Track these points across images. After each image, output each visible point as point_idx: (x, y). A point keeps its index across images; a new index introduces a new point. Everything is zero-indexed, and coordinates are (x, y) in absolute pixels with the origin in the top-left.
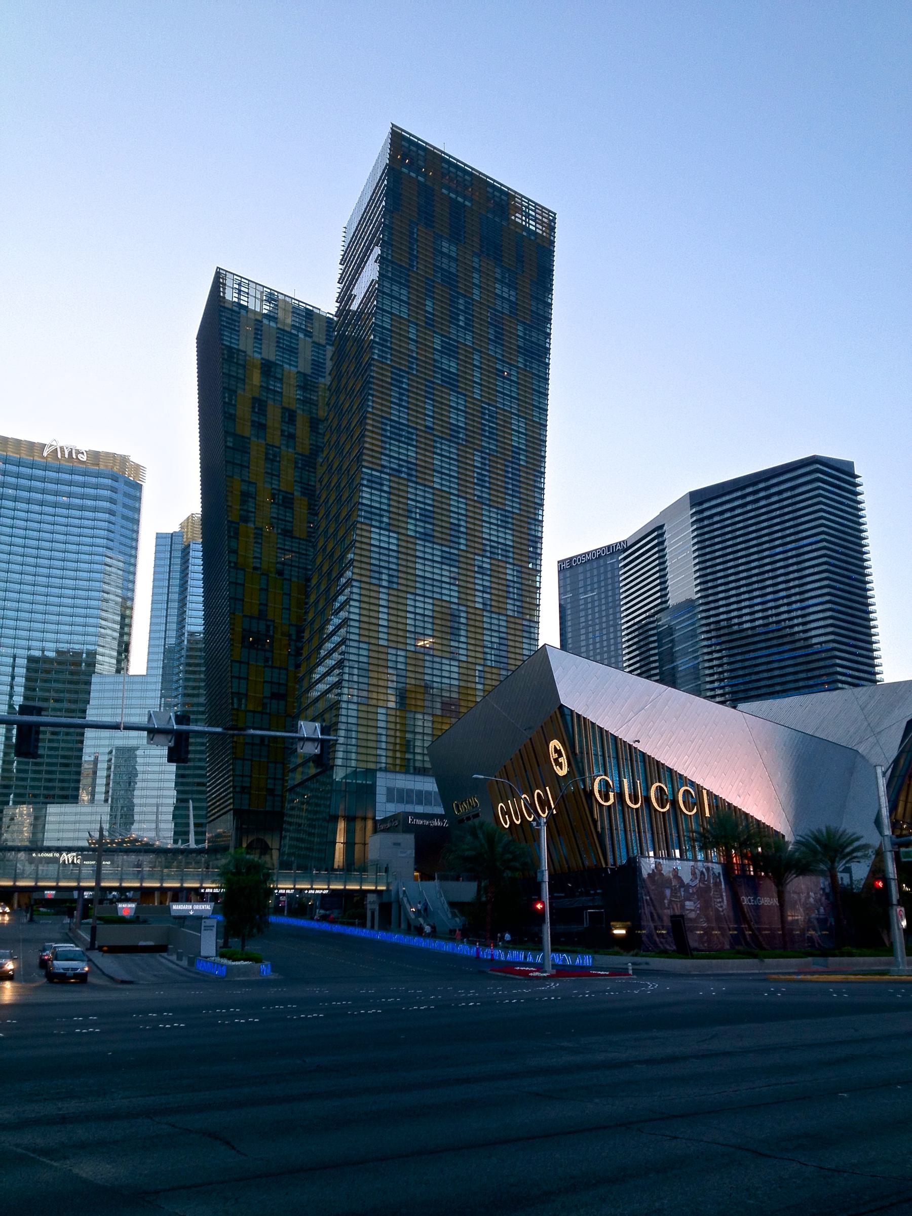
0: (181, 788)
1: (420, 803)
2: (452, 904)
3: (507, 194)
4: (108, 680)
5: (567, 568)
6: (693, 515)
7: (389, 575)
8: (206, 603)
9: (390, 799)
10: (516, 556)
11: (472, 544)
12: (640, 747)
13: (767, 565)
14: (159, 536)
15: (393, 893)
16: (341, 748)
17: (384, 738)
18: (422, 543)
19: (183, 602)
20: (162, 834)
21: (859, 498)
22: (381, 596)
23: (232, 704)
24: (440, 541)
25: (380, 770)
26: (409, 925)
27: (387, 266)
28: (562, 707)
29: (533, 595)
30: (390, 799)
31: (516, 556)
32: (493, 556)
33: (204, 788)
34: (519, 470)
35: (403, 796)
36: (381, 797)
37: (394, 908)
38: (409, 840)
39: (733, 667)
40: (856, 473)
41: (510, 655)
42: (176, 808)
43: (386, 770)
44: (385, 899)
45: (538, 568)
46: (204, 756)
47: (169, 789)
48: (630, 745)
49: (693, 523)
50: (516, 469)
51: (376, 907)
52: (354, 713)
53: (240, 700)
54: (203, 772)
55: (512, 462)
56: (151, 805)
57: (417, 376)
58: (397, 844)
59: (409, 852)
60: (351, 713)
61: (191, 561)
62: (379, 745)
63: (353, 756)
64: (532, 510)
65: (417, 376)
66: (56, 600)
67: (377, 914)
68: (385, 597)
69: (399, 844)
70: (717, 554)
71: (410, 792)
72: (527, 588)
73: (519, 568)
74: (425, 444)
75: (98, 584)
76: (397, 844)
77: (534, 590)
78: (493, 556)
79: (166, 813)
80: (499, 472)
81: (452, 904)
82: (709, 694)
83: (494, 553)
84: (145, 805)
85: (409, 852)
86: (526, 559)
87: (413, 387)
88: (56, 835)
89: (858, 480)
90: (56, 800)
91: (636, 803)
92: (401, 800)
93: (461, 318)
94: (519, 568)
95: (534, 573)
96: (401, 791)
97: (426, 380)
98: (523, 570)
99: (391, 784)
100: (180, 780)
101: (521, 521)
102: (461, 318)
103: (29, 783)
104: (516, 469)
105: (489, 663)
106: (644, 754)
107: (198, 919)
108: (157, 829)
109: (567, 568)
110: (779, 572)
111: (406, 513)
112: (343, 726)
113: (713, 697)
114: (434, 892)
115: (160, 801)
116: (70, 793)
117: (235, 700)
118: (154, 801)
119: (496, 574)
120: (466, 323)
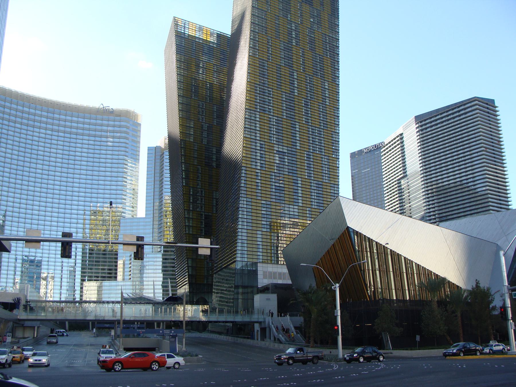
0: (165, 273)
1: (280, 279)
4: (128, 221)
5: (353, 155)
6: (417, 128)
7: (261, 144)
8: (172, 188)
9: (265, 277)
10: (326, 151)
11: (303, 146)
13: (458, 132)
14: (149, 149)
15: (267, 323)
16: (239, 252)
17: (261, 247)
18: (277, 146)
19: (161, 181)
20: (156, 295)
22: (258, 236)
23: (186, 231)
24: (286, 145)
25: (260, 262)
26: (275, 338)
27: (256, 35)
28: (348, 227)
29: (335, 162)
30: (265, 277)
31: (326, 151)
32: (314, 152)
33: (174, 273)
34: (326, 108)
35: (273, 275)
37: (267, 330)
38: (274, 297)
39: (441, 212)
40: (496, 105)
41: (324, 193)
42: (163, 282)
43: (262, 262)
44: (263, 326)
45: (338, 157)
46: (174, 257)
47: (159, 273)
48: (384, 246)
49: (417, 132)
50: (324, 107)
51: (259, 329)
52: (245, 234)
53: (189, 229)
54: (173, 265)
55: (322, 104)
56: (151, 281)
57: (272, 63)
58: (268, 299)
60: (243, 234)
61: (164, 190)
62: (258, 250)
63: (246, 256)
64: (333, 128)
65: (272, 63)
66: (103, 169)
67: (259, 333)
68: (260, 236)
69: (269, 299)
70: (431, 161)
71: (275, 273)
72: (332, 167)
73: (328, 158)
74: (278, 108)
75: (122, 165)
76: (268, 299)
77: (336, 168)
78: (314, 152)
79: (158, 285)
80: (315, 108)
82: (428, 218)
83: (314, 133)
84: (148, 281)
86: (331, 153)
87: (270, 85)
88: (107, 296)
89: (497, 109)
90: (107, 279)
92: (270, 278)
93: (293, 33)
94: (328, 158)
95: (336, 160)
96: (270, 273)
97: (277, 64)
98: (330, 158)
99: (265, 270)
100: (164, 269)
101: (328, 133)
102: (293, 33)
103: (94, 271)
104: (324, 107)
105: (314, 207)
108: (154, 293)
109: (353, 155)
110: (469, 180)
111: (268, 122)
112: (240, 241)
113: (430, 220)
114: (287, 321)
115: (155, 279)
116: (113, 275)
117: (187, 229)
118: (152, 279)
119: (316, 161)
120: (298, 94)
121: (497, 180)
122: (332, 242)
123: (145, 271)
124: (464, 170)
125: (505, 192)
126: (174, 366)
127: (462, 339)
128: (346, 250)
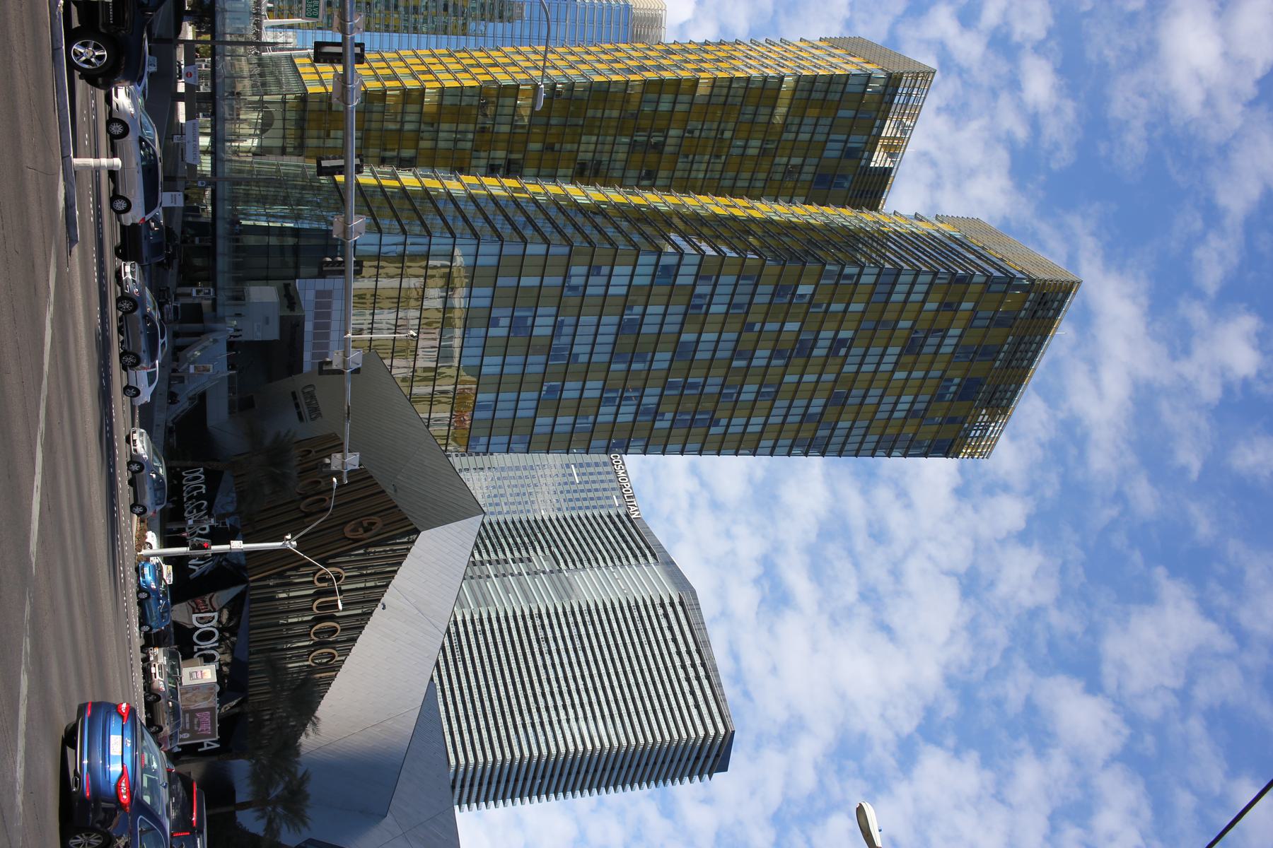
1: (316, 326)
2: (202, 397)
3: (1008, 406)
9: (319, 294)
12: (378, 610)
21: (686, 779)
28: (417, 532)
30: (319, 294)
36: (320, 284)
38: (272, 333)
40: (715, 775)
48: (379, 600)
59: (259, 334)
71: (328, 315)
81: (202, 397)
85: (259, 334)
89: (706, 777)
91: (318, 608)
92: (318, 305)
96: (329, 305)
106: (371, 614)
107: (149, 779)
121: (525, 779)
122: (390, 491)
123: (251, 683)
124: (581, 687)
125: (491, 795)
126: (134, 473)
127: (211, 812)
128: (374, 526)
